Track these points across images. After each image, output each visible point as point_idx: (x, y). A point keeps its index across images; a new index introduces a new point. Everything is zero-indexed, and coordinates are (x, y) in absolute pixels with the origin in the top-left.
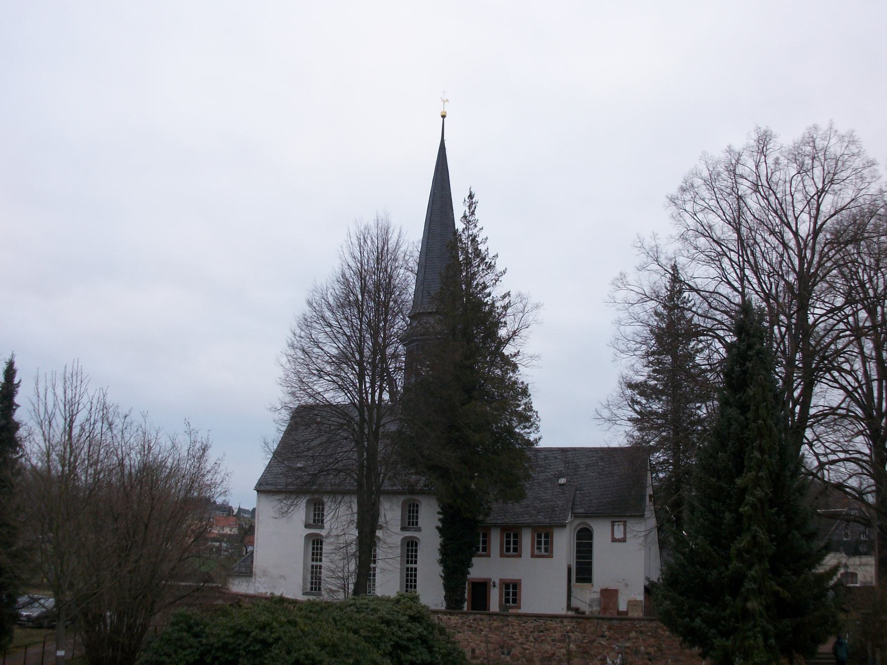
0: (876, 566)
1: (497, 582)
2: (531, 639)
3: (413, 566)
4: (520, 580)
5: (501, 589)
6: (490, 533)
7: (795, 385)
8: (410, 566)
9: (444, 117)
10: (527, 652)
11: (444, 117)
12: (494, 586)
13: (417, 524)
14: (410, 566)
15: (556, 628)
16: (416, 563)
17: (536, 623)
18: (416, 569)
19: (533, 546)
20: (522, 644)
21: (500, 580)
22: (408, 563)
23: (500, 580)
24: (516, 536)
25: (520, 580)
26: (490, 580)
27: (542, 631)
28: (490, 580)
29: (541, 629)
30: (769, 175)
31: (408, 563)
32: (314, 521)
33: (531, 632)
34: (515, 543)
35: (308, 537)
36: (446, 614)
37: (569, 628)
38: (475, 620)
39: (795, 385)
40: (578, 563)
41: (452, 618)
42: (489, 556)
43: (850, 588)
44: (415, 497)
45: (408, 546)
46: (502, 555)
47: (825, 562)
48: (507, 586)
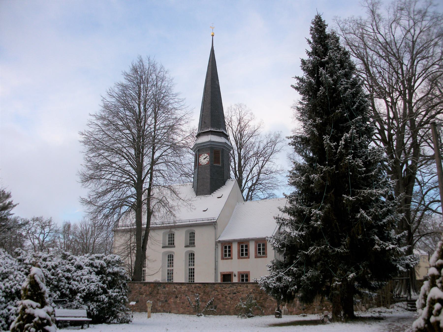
1: (237, 274)
2: (229, 298)
4: (249, 272)
5: (239, 277)
7: (412, 151)
9: (213, 36)
10: (226, 306)
11: (213, 36)
13: (194, 244)
15: (244, 291)
17: (232, 288)
18: (194, 269)
19: (222, 253)
20: (223, 301)
21: (238, 272)
23: (238, 272)
25: (249, 272)
27: (235, 293)
28: (233, 272)
29: (235, 291)
32: (169, 244)
33: (229, 294)
34: (264, 249)
35: (186, 252)
36: (179, 285)
37: (251, 290)
38: (195, 287)
39: (412, 151)
41: (183, 287)
42: (249, 258)
44: (173, 230)
46: (239, 258)
47: (143, 222)
48: (243, 276)
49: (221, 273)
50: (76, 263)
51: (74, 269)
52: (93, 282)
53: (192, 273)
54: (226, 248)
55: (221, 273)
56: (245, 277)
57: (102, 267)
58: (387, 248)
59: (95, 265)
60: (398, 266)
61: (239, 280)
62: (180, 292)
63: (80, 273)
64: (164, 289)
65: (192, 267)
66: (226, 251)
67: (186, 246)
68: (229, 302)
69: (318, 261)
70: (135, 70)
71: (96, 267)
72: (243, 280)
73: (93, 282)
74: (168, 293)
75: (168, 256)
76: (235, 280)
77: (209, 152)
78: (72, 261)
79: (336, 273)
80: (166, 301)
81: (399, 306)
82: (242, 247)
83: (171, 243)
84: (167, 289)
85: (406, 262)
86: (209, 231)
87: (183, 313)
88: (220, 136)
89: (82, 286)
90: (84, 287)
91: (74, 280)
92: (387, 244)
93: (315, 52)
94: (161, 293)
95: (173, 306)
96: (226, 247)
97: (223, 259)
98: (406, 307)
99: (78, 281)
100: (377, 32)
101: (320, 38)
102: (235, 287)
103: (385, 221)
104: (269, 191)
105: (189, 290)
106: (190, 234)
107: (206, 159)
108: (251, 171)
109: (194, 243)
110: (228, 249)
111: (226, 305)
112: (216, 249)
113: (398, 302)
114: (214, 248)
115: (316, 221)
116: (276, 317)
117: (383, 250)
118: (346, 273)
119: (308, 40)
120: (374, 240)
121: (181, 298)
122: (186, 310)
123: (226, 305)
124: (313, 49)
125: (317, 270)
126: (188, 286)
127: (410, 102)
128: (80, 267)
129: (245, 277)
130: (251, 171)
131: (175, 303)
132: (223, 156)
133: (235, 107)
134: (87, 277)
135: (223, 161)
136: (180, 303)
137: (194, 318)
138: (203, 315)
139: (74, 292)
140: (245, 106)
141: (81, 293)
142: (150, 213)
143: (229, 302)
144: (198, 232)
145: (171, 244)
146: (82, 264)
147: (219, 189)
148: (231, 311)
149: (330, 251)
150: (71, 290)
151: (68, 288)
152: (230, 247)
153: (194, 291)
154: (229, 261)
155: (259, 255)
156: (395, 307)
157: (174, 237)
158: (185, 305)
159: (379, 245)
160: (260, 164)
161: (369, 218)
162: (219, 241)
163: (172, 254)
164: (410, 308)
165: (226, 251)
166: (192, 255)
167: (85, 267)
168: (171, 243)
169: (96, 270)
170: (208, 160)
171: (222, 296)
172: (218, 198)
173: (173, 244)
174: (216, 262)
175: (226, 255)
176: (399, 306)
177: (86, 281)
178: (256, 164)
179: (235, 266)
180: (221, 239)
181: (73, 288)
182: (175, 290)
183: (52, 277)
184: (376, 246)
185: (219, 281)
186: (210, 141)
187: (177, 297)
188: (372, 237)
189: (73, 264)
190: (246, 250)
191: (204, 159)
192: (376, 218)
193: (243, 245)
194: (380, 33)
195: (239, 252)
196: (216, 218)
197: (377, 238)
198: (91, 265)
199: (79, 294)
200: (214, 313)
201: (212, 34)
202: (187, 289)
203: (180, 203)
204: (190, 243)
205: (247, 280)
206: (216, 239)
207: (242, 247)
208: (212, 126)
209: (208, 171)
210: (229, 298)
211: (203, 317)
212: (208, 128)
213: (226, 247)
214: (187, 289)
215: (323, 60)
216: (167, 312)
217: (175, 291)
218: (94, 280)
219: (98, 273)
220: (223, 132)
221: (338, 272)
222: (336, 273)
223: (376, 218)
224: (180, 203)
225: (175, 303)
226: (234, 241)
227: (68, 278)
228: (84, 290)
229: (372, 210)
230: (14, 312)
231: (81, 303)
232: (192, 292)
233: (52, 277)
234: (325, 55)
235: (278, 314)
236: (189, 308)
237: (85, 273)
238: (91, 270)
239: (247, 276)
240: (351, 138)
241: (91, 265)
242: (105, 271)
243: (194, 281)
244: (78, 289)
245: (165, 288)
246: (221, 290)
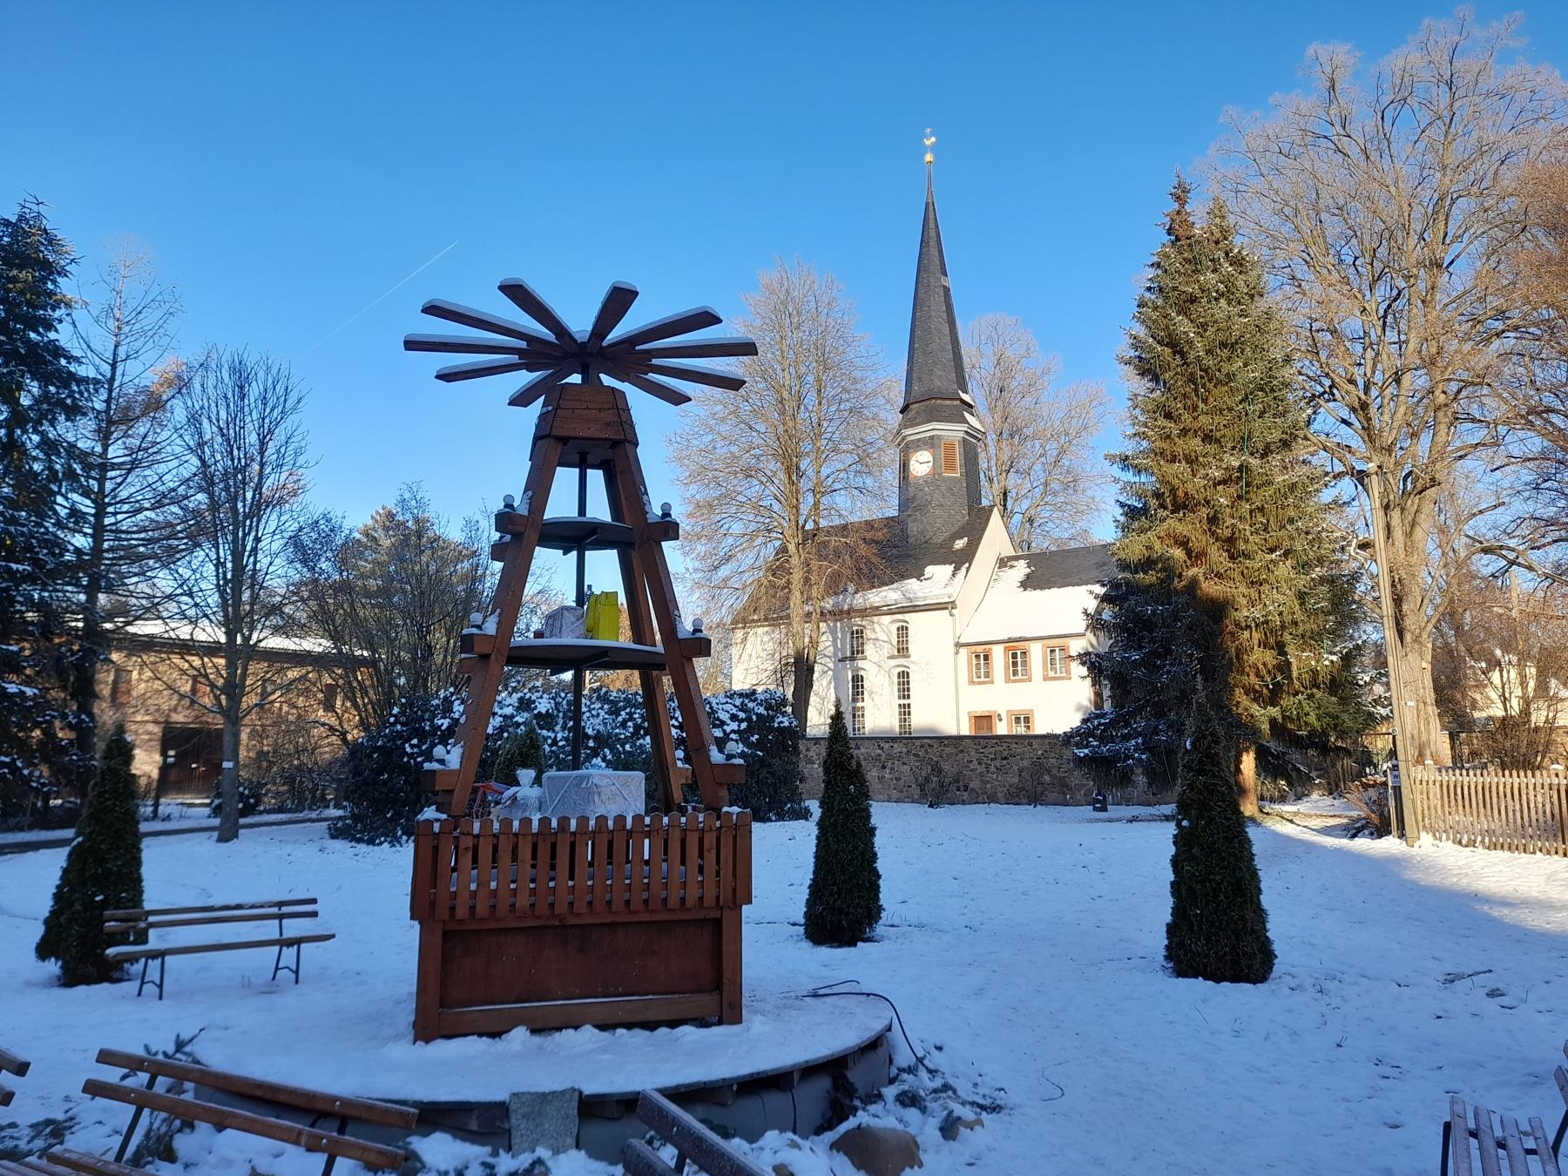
2: (993, 769)
3: (902, 702)
44: (906, 617)
46: (1008, 680)
53: (905, 711)
62: (890, 757)
82: (1014, 656)
116: (1095, 809)
124: (134, 776)
155: (1051, 674)
166: (904, 677)
187: (884, 767)
195: (1007, 669)
207: (1014, 656)
210: (993, 769)
235: (1099, 801)
239: (1027, 720)
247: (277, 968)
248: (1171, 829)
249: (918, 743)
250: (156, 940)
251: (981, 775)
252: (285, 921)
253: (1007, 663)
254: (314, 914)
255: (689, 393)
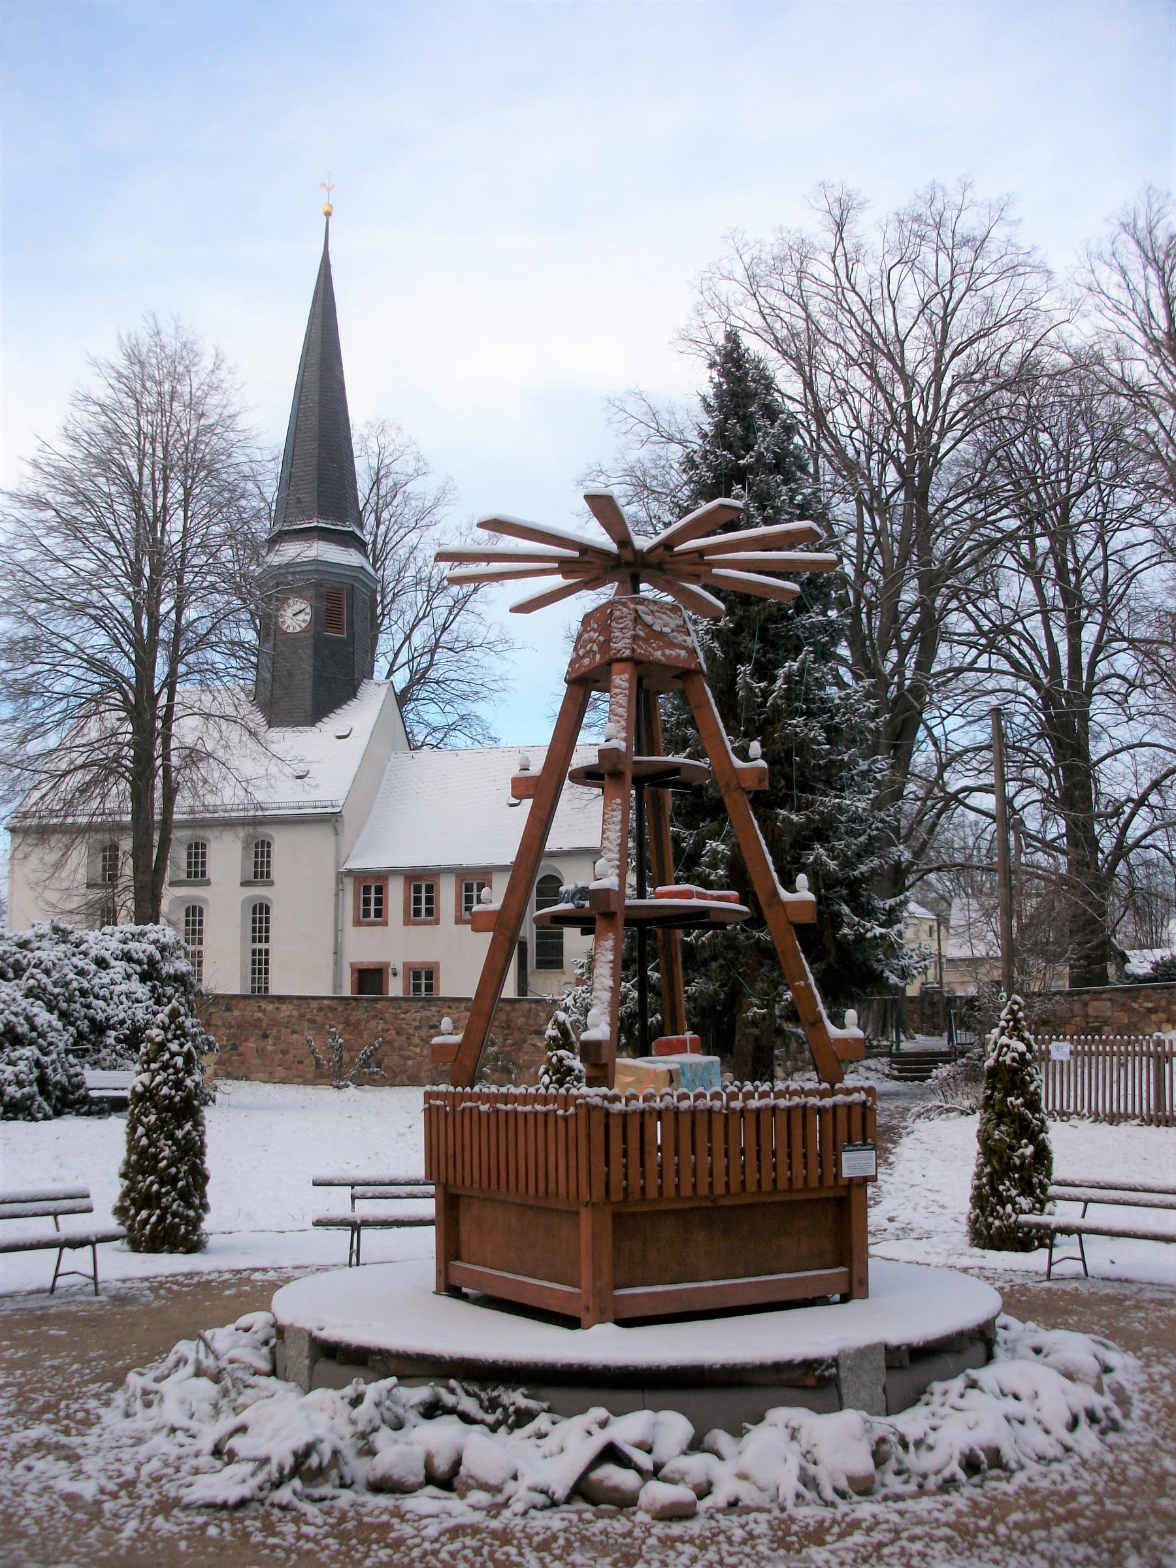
0: (656, 1409)
2: (416, 1040)
3: (263, 946)
4: (437, 964)
6: (438, 884)
8: (258, 946)
9: (328, 214)
10: (410, 1062)
11: (328, 214)
12: (395, 975)
13: (268, 876)
14: (258, 946)
16: (267, 940)
18: (267, 952)
19: (356, 907)
21: (405, 964)
22: (254, 941)
23: (405, 964)
24: (430, 889)
25: (437, 964)
26: (388, 964)
28: (388, 964)
30: (1147, 244)
31: (254, 941)
33: (416, 1028)
35: (245, 902)
38: (320, 1009)
40: (539, 936)
41: (284, 1007)
42: (437, 923)
43: (841, 1265)
44: (201, 833)
45: (254, 913)
46: (407, 922)
48: (417, 976)
49: (352, 965)
50: (93, 953)
51: (93, 967)
52: (138, 1001)
53: (260, 964)
54: (369, 893)
55: (352, 965)
56: (423, 977)
57: (152, 961)
58: (869, 935)
59: (135, 956)
60: (887, 973)
61: (406, 991)
62: (274, 1023)
63: (105, 977)
64: (227, 1014)
65: (263, 946)
66: (367, 902)
67: (245, 884)
68: (418, 1050)
69: (715, 958)
70: (135, 358)
71: (139, 962)
72: (417, 988)
73: (138, 1001)
74: (239, 1026)
75: (187, 910)
76: (396, 987)
77: (310, 593)
78: (83, 947)
79: (752, 987)
80: (235, 1047)
81: (869, 1069)
82: (417, 889)
83: (196, 874)
84: (237, 1013)
85: (903, 962)
86: (317, 840)
87: (284, 1081)
88: (346, 545)
89: (118, 1012)
90: (122, 1015)
91: (97, 997)
92: (868, 925)
93: (721, 436)
94: (219, 1023)
95: (257, 1061)
96: (367, 890)
97: (357, 923)
98: (887, 1070)
99: (105, 1000)
100: (847, 285)
101: (733, 394)
102: (434, 1009)
103: (863, 868)
104: (463, 708)
105: (301, 1016)
106: (257, 846)
107: (301, 617)
108: (408, 638)
109: (268, 873)
110: (373, 896)
111: (409, 1058)
112: (337, 895)
113: (867, 1058)
114: (332, 891)
115: (713, 866)
117: (860, 938)
118: (776, 988)
119: (704, 399)
120: (839, 914)
121: (277, 1038)
122: (294, 1071)
123: (409, 1058)
125: (710, 979)
126: (298, 1007)
127: (924, 499)
128: (102, 963)
129: (423, 977)
130: (408, 638)
131: (261, 1052)
132: (351, 607)
133: (365, 432)
134: (123, 988)
135: (351, 623)
136: (276, 1052)
137: (325, 1094)
138: (352, 1087)
139: (99, 1028)
140: (399, 429)
141: (115, 1029)
142: (170, 793)
143: (418, 1050)
144: (283, 843)
145: (196, 875)
146: (107, 955)
147: (339, 711)
148: (423, 1075)
149: (742, 937)
150: (92, 1020)
151: (86, 1017)
152: (379, 890)
153: (318, 1019)
154: (378, 929)
156: (861, 1070)
157: (204, 855)
158: (290, 1057)
159: (851, 926)
160: (440, 616)
161: (833, 865)
162: (350, 871)
163: (197, 904)
164: (896, 1073)
165: (367, 902)
167: (113, 963)
168: (196, 874)
169: (138, 969)
170: (308, 618)
171: (398, 1033)
172: (339, 737)
173: (203, 874)
174: (338, 931)
175: (366, 914)
176: (869, 1069)
177: (123, 998)
178: (424, 617)
179: (394, 944)
180: (355, 864)
181: (98, 1018)
182: (260, 1015)
183: (57, 990)
184: (846, 930)
185: (347, 992)
186: (316, 561)
187: (265, 1036)
188: (836, 907)
189: (85, 954)
190: (429, 900)
191: (296, 617)
192: (847, 863)
193: (422, 885)
194: (854, 290)
196: (341, 803)
197: (845, 909)
198: (127, 957)
199: (113, 1033)
200: (374, 1082)
201: (326, 209)
202: (295, 1013)
203: (273, 769)
204: (256, 873)
205: (429, 988)
206: (337, 865)
207: (417, 889)
208: (322, 513)
209: (307, 653)
210: (416, 1040)
211: (352, 1090)
212: (310, 518)
213: (367, 890)
214: (295, 1013)
215: (741, 462)
216: (237, 1078)
217: (259, 1020)
218: (139, 995)
219: (144, 978)
220: (352, 533)
221: (759, 985)
222: (752, 987)
223: (847, 863)
224: (273, 767)
225: (261, 1052)
226: (396, 871)
227: (84, 993)
228: (122, 1022)
229: (839, 845)
230: (12, 1077)
231: (122, 1056)
232: (312, 1021)
233: (57, 990)
234: (749, 448)
236: (301, 1067)
237: (118, 978)
238: (130, 971)
239: (430, 975)
240: (801, 671)
241: (127, 957)
242: (159, 971)
243: (267, 989)
244: (108, 1019)
245: (229, 1009)
246: (396, 1016)
247: (56, 1276)
248: (972, 1124)
249: (314, 1004)
250: (1063, 1213)
251: (401, 1049)
252: (60, 1217)
253: (407, 899)
254: (89, 1210)
255: (484, 534)
